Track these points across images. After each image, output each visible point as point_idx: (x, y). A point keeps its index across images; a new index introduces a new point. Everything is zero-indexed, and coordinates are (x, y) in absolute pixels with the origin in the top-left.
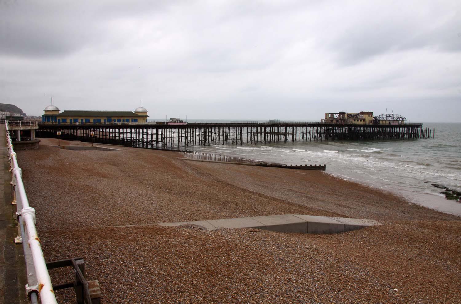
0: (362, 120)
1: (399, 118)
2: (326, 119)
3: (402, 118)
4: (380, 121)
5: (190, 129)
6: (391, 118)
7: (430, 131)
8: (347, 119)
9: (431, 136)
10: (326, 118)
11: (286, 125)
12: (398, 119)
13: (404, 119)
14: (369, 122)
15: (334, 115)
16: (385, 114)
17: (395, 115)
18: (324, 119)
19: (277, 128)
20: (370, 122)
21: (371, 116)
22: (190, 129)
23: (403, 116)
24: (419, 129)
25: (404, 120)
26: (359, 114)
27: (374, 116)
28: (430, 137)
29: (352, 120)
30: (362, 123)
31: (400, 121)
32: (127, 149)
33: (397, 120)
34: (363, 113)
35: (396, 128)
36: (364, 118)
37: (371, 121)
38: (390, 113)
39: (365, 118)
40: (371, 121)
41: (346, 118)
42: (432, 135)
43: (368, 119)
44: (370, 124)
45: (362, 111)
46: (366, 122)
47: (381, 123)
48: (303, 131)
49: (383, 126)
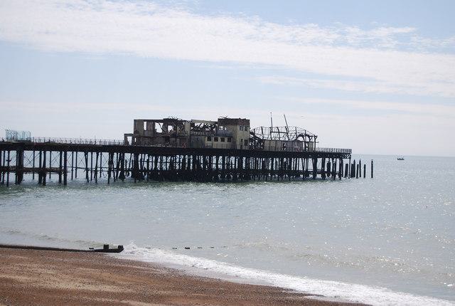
0: (226, 139)
3: (309, 136)
4: (266, 142)
6: (282, 135)
11: (63, 148)
17: (291, 130)
18: (130, 135)
19: (40, 153)
22: (87, 173)
26: (216, 123)
27: (251, 130)
30: (224, 145)
32: (240, 270)
34: (225, 122)
35: (7, 152)
46: (235, 142)
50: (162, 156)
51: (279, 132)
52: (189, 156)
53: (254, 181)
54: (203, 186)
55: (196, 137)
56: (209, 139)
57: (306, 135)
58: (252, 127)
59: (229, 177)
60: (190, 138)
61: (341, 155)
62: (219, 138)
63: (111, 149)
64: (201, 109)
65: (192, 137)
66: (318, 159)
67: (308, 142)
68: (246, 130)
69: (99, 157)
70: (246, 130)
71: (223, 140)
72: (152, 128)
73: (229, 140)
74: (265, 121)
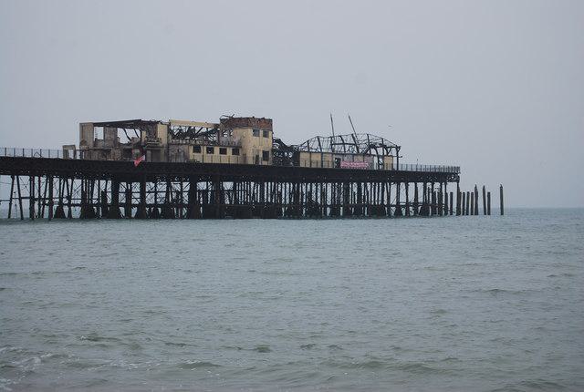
0: (229, 151)
1: (374, 146)
2: (84, 147)
5: (10, 204)
6: (347, 146)
7: (489, 193)
8: (169, 144)
9: (491, 207)
10: (82, 143)
12: (373, 152)
13: (394, 150)
14: (257, 156)
15: (120, 131)
16: (326, 133)
17: (362, 138)
20: (261, 156)
21: (266, 135)
22: (10, 204)
23: (391, 139)
24: (451, 187)
25: (394, 152)
27: (276, 136)
28: (487, 211)
29: (186, 147)
30: (230, 158)
31: (378, 157)
33: (370, 155)
34: (231, 123)
36: (236, 140)
37: (265, 154)
38: (344, 130)
39: (240, 142)
40: (265, 154)
41: (164, 141)
42: (495, 204)
43: (254, 146)
45: (370, 127)
46: (245, 157)
47: (304, 161)
48: (22, 215)
49: (318, 175)
50: (282, 182)
51: (344, 144)
52: (340, 184)
54: (223, 221)
56: (197, 149)
58: (278, 132)
59: (408, 212)
61: (448, 175)
64: (185, 100)
68: (266, 135)
69: (15, 181)
71: (223, 152)
72: (113, 137)
73: (236, 151)
74: (301, 126)
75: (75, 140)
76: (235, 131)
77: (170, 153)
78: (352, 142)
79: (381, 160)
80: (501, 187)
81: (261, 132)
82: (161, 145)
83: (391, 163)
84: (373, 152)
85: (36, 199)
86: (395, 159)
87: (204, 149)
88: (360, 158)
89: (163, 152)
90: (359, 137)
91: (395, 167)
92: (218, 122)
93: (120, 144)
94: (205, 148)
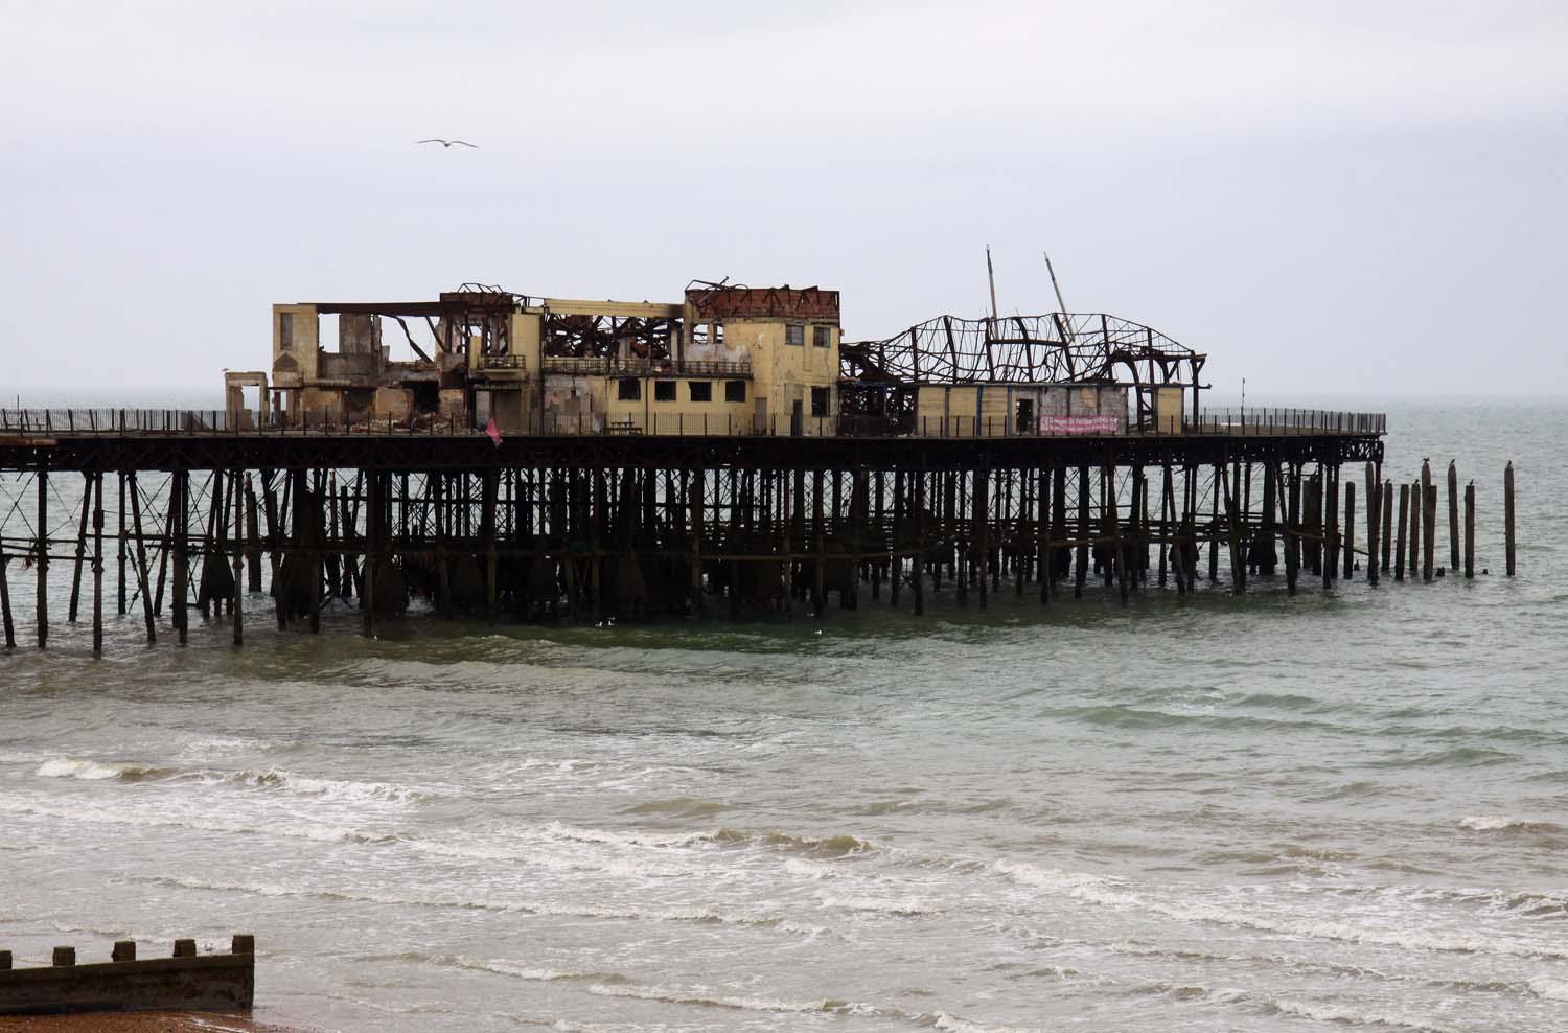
0: (718, 389)
2: (289, 377)
3: (1162, 359)
7: (1470, 490)
8: (544, 373)
10: (283, 363)
12: (1121, 373)
13: (1185, 365)
14: (798, 405)
16: (971, 307)
17: (1085, 327)
23: (1175, 335)
24: (1352, 472)
26: (676, 310)
27: (851, 337)
29: (598, 383)
30: (716, 415)
31: (1140, 389)
34: (720, 303)
36: (734, 356)
37: (819, 394)
39: (747, 361)
40: (819, 394)
43: (785, 371)
44: (812, 427)
47: (930, 412)
53: (1058, 621)
55: (567, 383)
57: (1151, 354)
60: (542, 391)
62: (683, 388)
63: (173, 445)
65: (552, 382)
66: (234, 538)
67: (1154, 389)
68: (820, 341)
70: (820, 341)
72: (367, 343)
74: (921, 275)
75: (262, 358)
76: (730, 327)
77: (549, 398)
78: (1055, 337)
79: (1147, 397)
80: (1509, 473)
81: (809, 331)
82: (522, 376)
83: (1172, 410)
84: (1121, 373)
85: (454, 502)
86: (1189, 391)
87: (648, 388)
88: (1089, 396)
89: (527, 392)
90: (1077, 324)
91: (769, 432)
92: (680, 300)
93: (390, 366)
94: (652, 383)
